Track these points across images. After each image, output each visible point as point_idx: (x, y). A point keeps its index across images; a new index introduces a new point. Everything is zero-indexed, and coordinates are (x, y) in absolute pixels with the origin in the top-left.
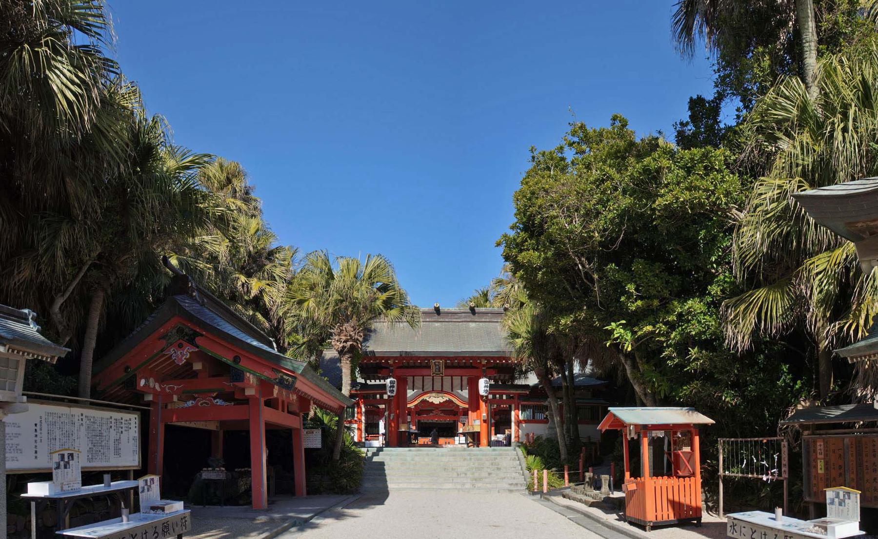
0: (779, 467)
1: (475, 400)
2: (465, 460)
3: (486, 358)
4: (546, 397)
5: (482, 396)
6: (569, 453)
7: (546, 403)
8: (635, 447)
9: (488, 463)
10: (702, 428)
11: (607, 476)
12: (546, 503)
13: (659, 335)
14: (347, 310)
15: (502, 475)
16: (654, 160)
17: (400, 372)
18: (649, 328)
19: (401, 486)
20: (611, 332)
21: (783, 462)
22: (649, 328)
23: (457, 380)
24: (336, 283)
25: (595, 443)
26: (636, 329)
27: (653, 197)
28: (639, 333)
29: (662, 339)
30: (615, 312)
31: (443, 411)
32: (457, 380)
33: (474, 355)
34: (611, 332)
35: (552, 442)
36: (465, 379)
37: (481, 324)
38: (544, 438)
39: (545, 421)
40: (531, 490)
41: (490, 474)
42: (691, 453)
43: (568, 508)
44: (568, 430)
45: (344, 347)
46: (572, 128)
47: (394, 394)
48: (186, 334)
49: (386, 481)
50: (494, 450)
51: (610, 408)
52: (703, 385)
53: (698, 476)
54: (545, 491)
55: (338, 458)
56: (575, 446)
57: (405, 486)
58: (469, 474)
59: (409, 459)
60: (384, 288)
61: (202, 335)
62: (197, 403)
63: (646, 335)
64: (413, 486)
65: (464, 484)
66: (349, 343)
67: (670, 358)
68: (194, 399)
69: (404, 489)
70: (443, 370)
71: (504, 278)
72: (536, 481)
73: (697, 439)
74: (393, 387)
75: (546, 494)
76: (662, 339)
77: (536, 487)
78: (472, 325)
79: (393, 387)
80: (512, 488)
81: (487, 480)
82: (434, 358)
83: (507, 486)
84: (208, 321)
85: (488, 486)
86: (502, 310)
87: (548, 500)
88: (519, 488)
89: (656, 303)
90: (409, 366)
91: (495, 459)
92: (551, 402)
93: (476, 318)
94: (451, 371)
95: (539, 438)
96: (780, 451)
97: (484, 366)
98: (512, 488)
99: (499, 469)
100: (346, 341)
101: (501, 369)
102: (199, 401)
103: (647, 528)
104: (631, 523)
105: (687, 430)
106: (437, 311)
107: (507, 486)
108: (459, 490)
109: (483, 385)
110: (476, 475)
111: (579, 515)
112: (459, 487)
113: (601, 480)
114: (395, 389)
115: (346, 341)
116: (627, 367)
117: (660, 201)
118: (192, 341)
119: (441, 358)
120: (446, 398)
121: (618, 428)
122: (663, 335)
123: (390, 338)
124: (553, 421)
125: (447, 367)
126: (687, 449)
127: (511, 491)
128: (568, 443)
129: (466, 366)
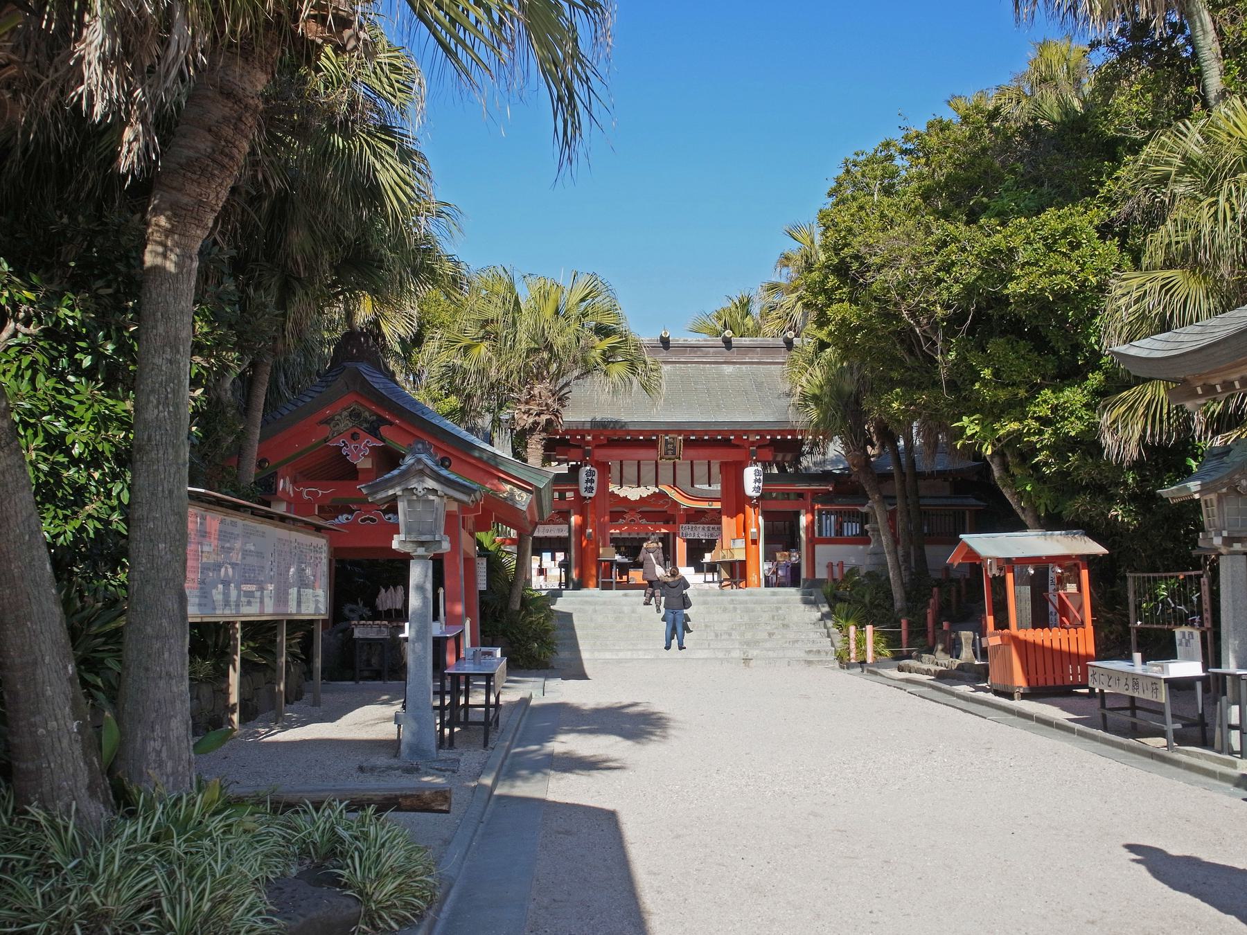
0: (1200, 613)
1: (736, 501)
2: (725, 610)
3: (758, 432)
4: (862, 496)
5: (751, 498)
6: (908, 597)
7: (864, 509)
8: (999, 583)
9: (766, 617)
10: (1090, 560)
11: (970, 634)
12: (874, 677)
13: (1029, 434)
14: (545, 362)
15: (791, 635)
16: (1005, 237)
17: (600, 454)
18: (1014, 426)
19: (621, 655)
20: (963, 429)
21: (1205, 607)
22: (1014, 426)
23: (701, 469)
24: (526, 322)
25: (958, 581)
26: (997, 426)
27: (1007, 278)
28: (1001, 432)
29: (1034, 439)
30: (970, 405)
31: (644, 514)
32: (701, 469)
33: (738, 428)
34: (963, 429)
35: (877, 579)
36: (716, 469)
37: (744, 367)
38: (863, 571)
39: (863, 538)
40: (843, 662)
41: (770, 635)
42: (1078, 593)
43: (908, 681)
44: (907, 556)
45: (536, 423)
46: (903, 133)
47: (592, 495)
48: (366, 420)
49: (579, 651)
50: (774, 594)
51: (961, 536)
52: (1093, 500)
53: (1089, 627)
54: (869, 661)
55: (518, 607)
56: (918, 588)
57: (629, 655)
58: (735, 635)
59: (626, 609)
60: (602, 331)
61: (391, 424)
62: (355, 519)
63: (1009, 433)
64: (641, 655)
65: (728, 651)
66: (544, 418)
67: (1046, 464)
68: (351, 512)
69: (627, 661)
70: (680, 449)
71: (783, 281)
72: (853, 646)
73: (1085, 574)
74: (592, 481)
75: (871, 665)
76: (1034, 439)
77: (852, 655)
78: (728, 369)
79: (592, 481)
80: (811, 657)
81: (768, 645)
82: (667, 432)
83: (803, 655)
84: (408, 407)
85: (771, 654)
86: (780, 341)
87: (876, 673)
88: (823, 657)
89: (1022, 393)
90: (615, 440)
91: (778, 609)
92: (872, 505)
93: (733, 356)
94: (692, 453)
95: (853, 571)
96: (1199, 590)
97: (753, 444)
98: (811, 657)
99: (786, 626)
100: (538, 415)
101: (780, 447)
102: (359, 516)
103: (1016, 695)
104: (997, 693)
105: (1072, 564)
106: (665, 343)
107: (803, 655)
108: (722, 660)
109: (751, 479)
110: (749, 636)
111: (925, 689)
112: (720, 655)
113: (960, 639)
114: (595, 485)
115: (538, 415)
116: (993, 466)
117: (1012, 287)
118: (374, 431)
119: (679, 432)
120: (652, 489)
121: (975, 564)
122: (1035, 434)
123: (594, 401)
124: (879, 542)
125: (688, 443)
126: (1072, 588)
127: (809, 663)
128: (906, 580)
129: (722, 446)
